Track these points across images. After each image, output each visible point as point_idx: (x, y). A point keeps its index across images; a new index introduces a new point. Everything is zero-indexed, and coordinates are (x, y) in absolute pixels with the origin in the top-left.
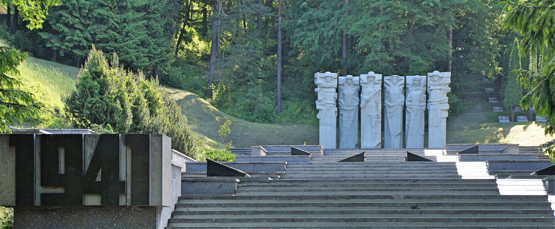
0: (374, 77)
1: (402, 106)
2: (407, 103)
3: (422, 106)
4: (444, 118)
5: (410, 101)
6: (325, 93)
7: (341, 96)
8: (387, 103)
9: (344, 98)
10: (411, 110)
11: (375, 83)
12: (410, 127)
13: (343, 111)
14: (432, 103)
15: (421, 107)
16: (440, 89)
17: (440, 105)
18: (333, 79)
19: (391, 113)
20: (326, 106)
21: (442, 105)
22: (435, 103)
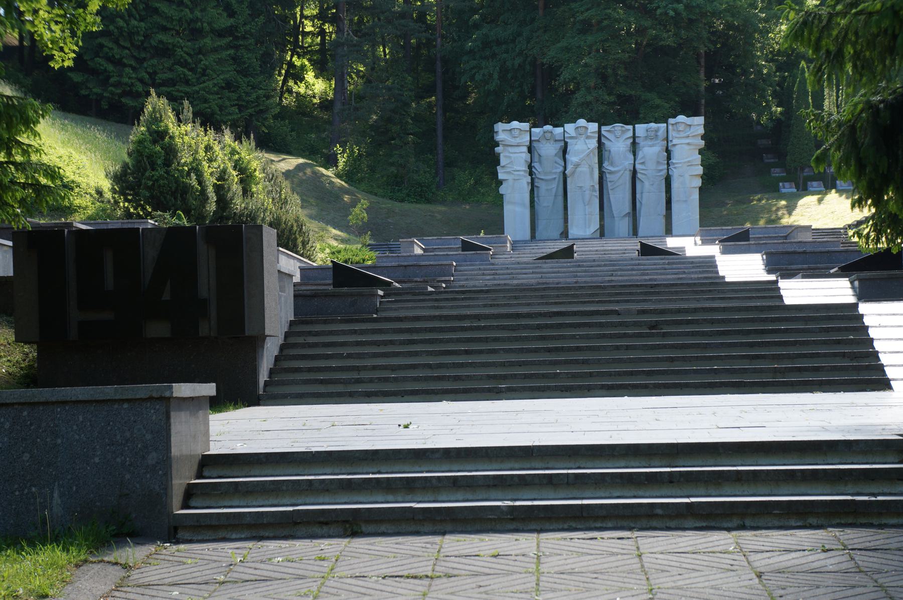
0: (586, 128)
1: (630, 171)
2: (638, 167)
3: (661, 170)
4: (696, 188)
5: (643, 163)
6: (511, 155)
7: (536, 158)
8: (607, 168)
9: (540, 162)
10: (644, 177)
11: (588, 137)
12: (643, 202)
13: (540, 181)
14: (676, 166)
15: (659, 172)
16: (688, 144)
17: (688, 168)
18: (523, 132)
19: (613, 183)
20: (513, 174)
21: (692, 167)
22: (680, 165)
